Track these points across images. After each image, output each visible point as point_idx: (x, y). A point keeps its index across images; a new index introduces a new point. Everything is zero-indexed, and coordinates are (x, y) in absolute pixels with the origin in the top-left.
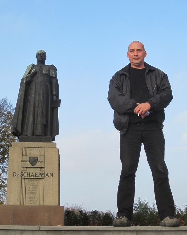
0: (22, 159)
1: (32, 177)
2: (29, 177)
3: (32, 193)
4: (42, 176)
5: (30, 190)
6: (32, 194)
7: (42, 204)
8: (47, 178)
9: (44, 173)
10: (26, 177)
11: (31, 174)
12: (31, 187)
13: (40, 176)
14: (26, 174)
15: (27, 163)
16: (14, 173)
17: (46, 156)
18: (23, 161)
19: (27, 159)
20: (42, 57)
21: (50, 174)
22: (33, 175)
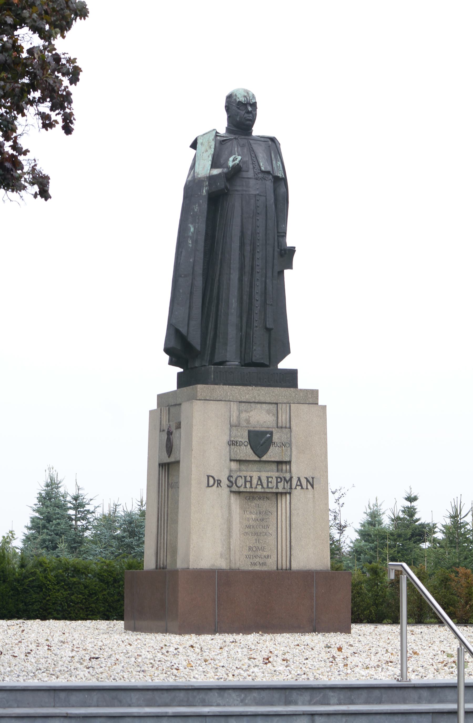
0: (230, 435)
1: (259, 489)
2: (251, 490)
3: (256, 534)
4: (284, 488)
5: (249, 527)
6: (256, 537)
7: (285, 565)
8: (297, 492)
9: (291, 478)
10: (242, 489)
11: (255, 481)
12: (253, 516)
13: (281, 485)
14: (241, 482)
15: (243, 447)
16: (208, 477)
17: (293, 428)
18: (232, 443)
19: (244, 437)
20: (241, 112)
21: (308, 481)
22: (262, 485)
